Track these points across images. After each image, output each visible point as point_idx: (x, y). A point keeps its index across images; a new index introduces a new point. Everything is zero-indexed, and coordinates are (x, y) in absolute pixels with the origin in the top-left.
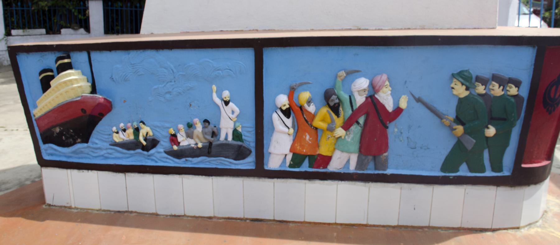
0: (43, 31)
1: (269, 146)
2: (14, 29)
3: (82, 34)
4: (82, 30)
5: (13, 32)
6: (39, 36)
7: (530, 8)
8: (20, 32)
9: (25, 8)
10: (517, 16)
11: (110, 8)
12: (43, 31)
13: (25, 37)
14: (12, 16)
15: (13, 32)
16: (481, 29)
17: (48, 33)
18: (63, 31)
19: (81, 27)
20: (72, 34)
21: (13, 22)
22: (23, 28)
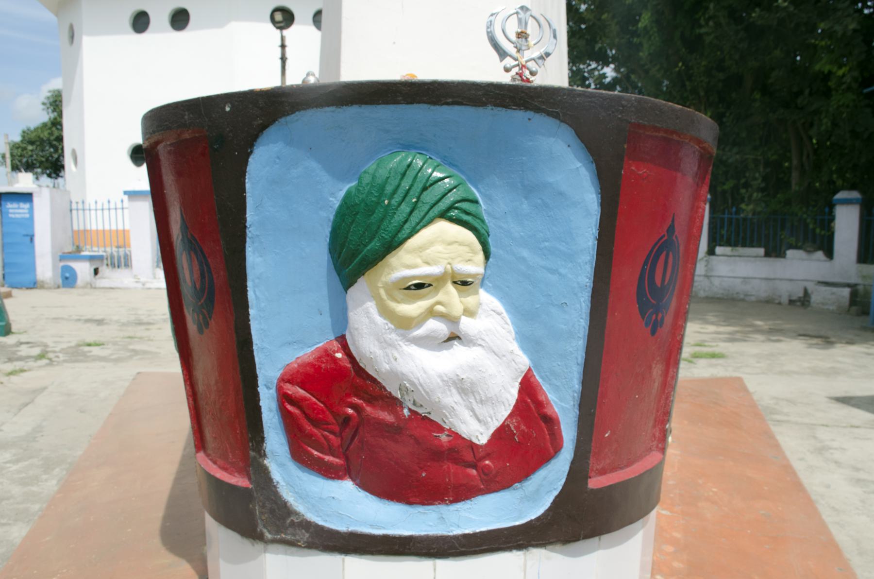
0: (761, 251)
1: (561, 553)
2: (720, 245)
3: (819, 260)
4: (820, 254)
5: (719, 250)
6: (753, 259)
7: (20, 223)
8: (727, 250)
9: (726, 216)
10: (764, 276)
11: (734, 216)
12: (761, 251)
13: (733, 258)
14: (722, 227)
15: (719, 250)
16: (88, 321)
17: (767, 254)
18: (790, 253)
19: (820, 248)
20: (803, 260)
21: (722, 236)
22: (735, 245)
